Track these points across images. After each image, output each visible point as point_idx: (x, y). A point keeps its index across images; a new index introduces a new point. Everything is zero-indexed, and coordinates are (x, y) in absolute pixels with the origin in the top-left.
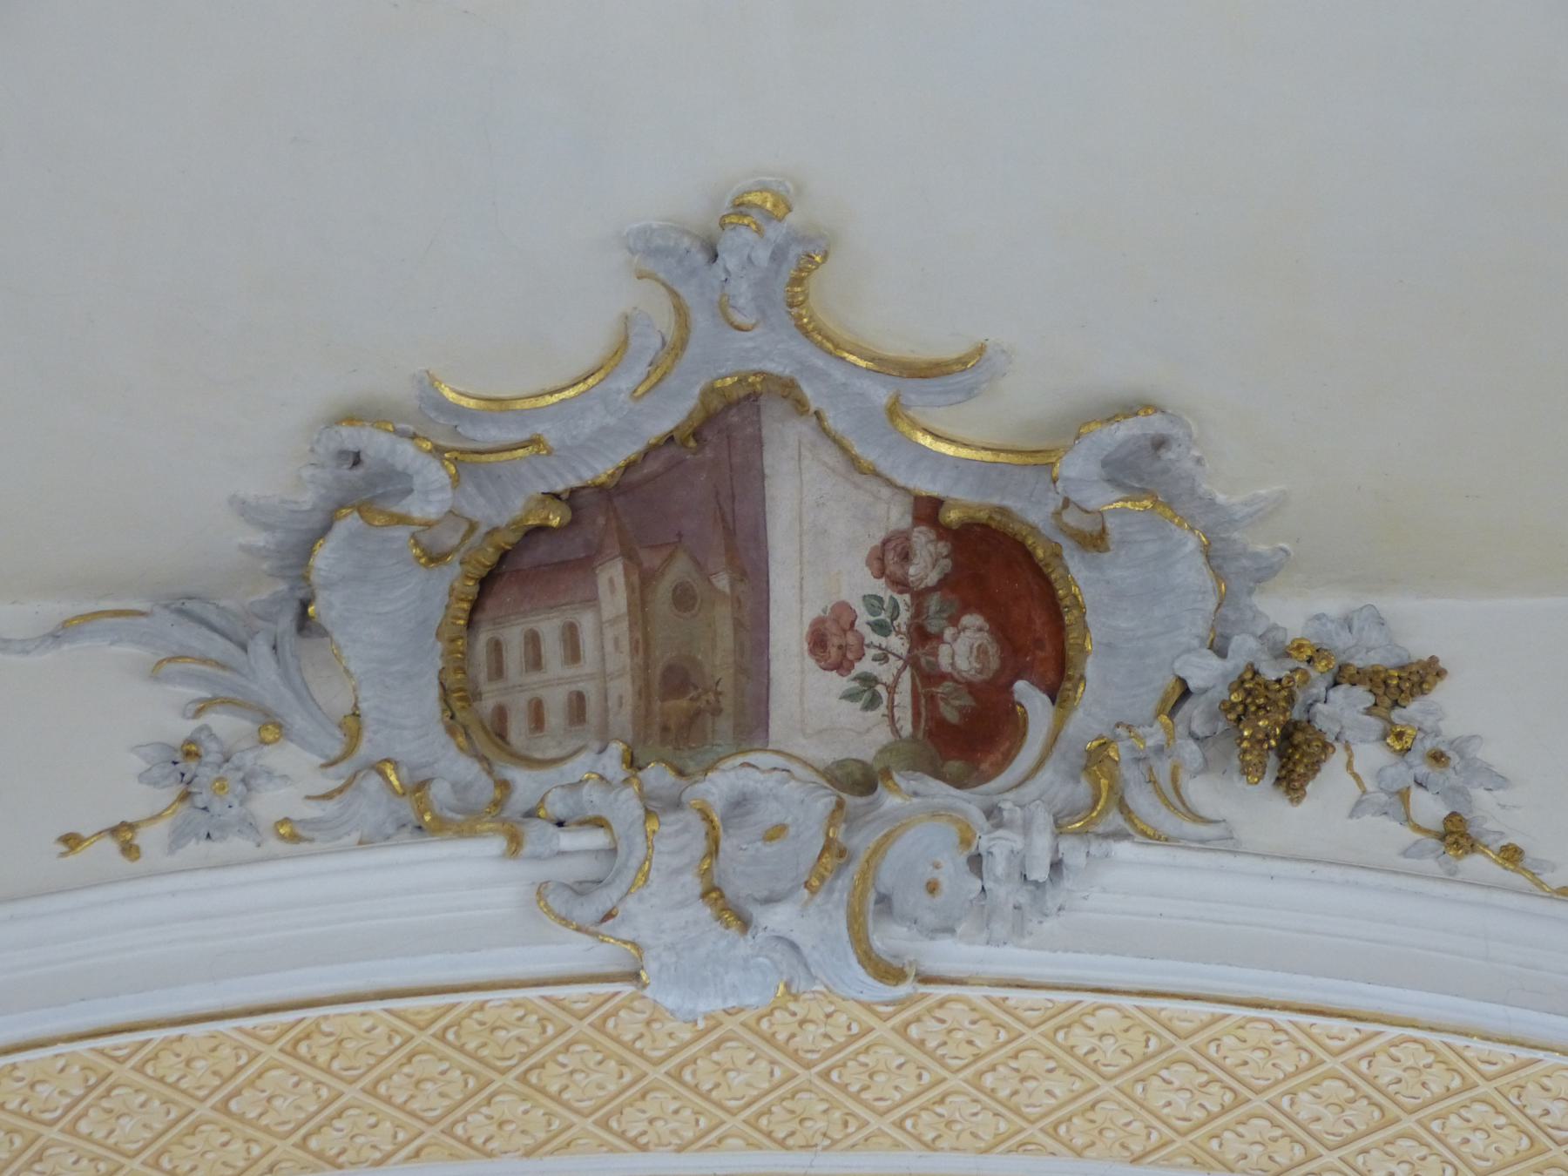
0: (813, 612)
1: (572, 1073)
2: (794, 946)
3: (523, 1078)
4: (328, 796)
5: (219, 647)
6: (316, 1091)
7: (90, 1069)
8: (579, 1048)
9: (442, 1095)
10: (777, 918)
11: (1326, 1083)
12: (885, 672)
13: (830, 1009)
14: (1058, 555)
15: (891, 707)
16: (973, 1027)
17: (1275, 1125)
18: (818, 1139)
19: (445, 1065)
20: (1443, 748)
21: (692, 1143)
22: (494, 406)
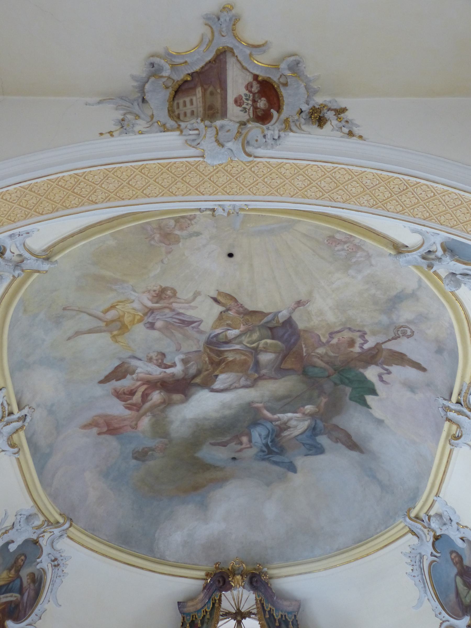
0: (235, 96)
1: (191, 178)
2: (232, 150)
3: (182, 179)
4: (148, 127)
5: (128, 104)
6: (145, 180)
7: (104, 173)
8: (192, 172)
9: (168, 182)
10: (229, 145)
11: (327, 179)
12: (248, 107)
13: (238, 164)
14: (279, 87)
15: (249, 113)
16: (264, 168)
17: (317, 188)
18: (235, 193)
19: (168, 176)
20: (348, 120)
21: (212, 193)
22: (178, 54)
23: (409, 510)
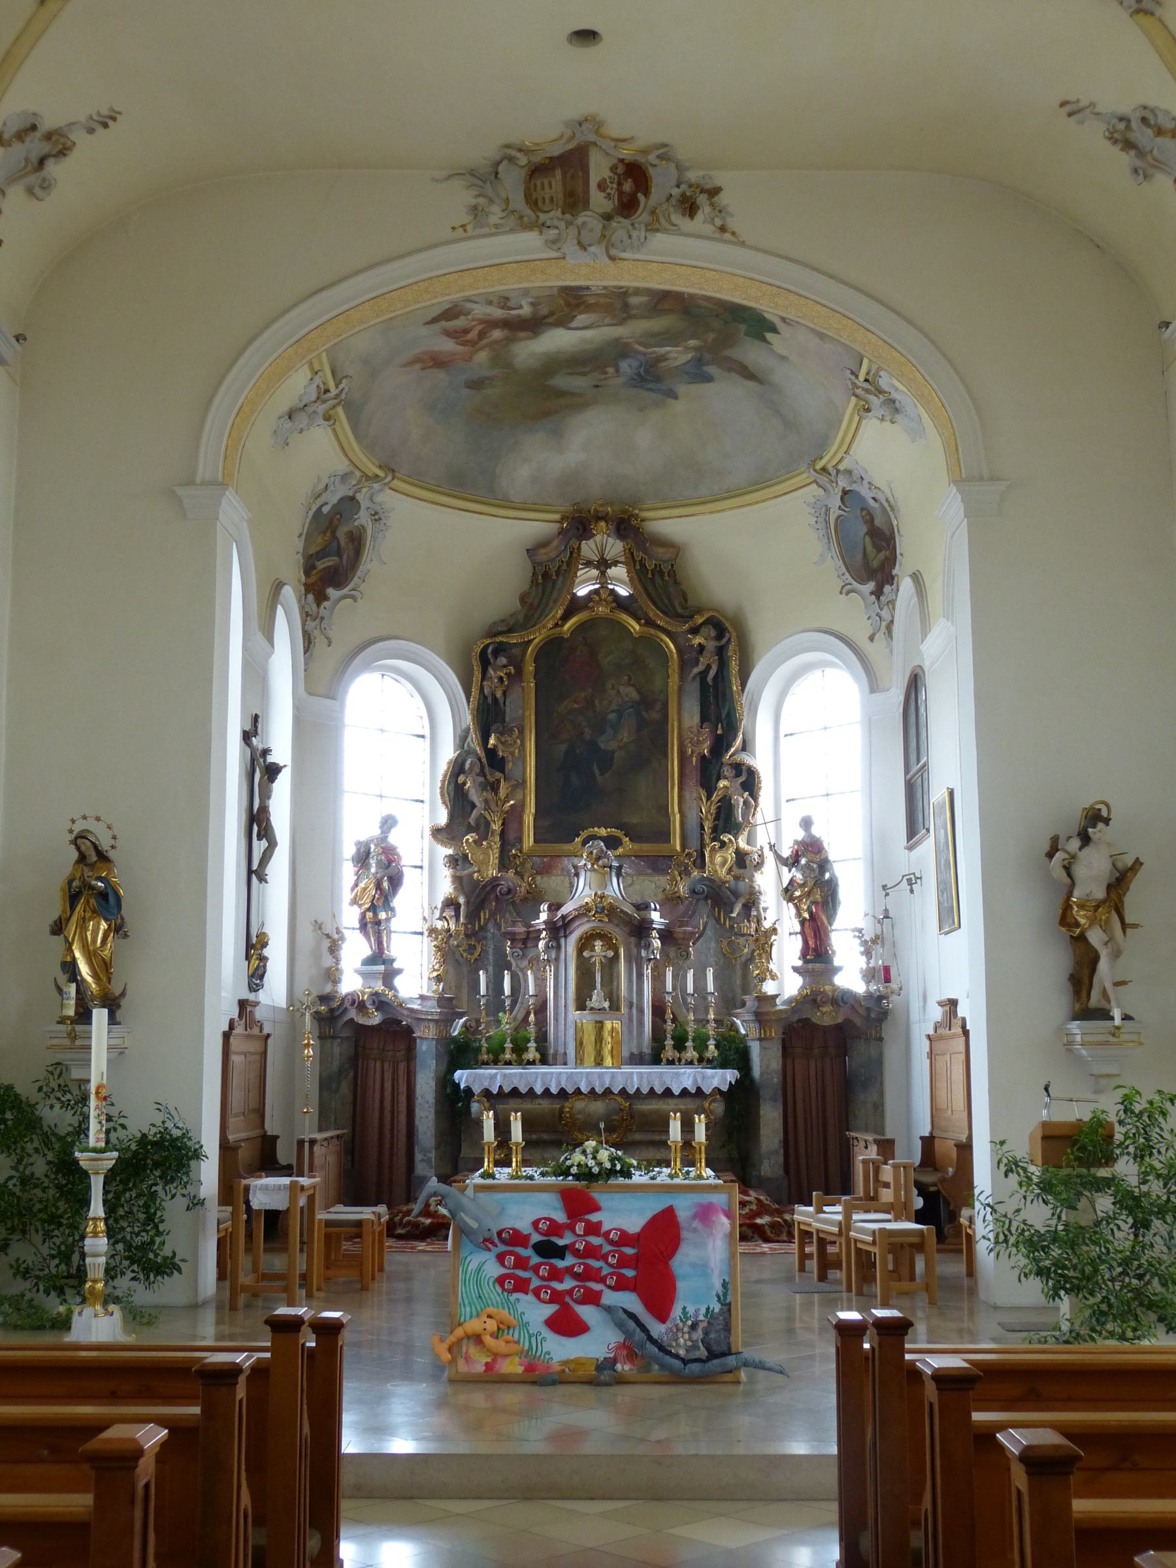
10: (592, 249)
12: (612, 192)
23: (814, 462)
